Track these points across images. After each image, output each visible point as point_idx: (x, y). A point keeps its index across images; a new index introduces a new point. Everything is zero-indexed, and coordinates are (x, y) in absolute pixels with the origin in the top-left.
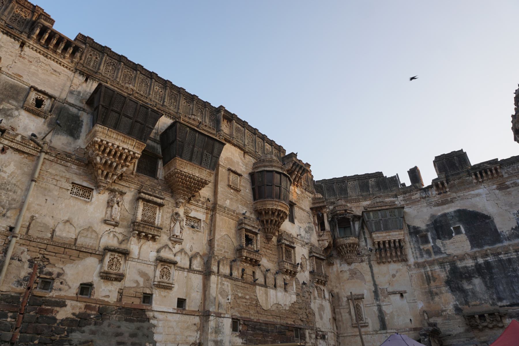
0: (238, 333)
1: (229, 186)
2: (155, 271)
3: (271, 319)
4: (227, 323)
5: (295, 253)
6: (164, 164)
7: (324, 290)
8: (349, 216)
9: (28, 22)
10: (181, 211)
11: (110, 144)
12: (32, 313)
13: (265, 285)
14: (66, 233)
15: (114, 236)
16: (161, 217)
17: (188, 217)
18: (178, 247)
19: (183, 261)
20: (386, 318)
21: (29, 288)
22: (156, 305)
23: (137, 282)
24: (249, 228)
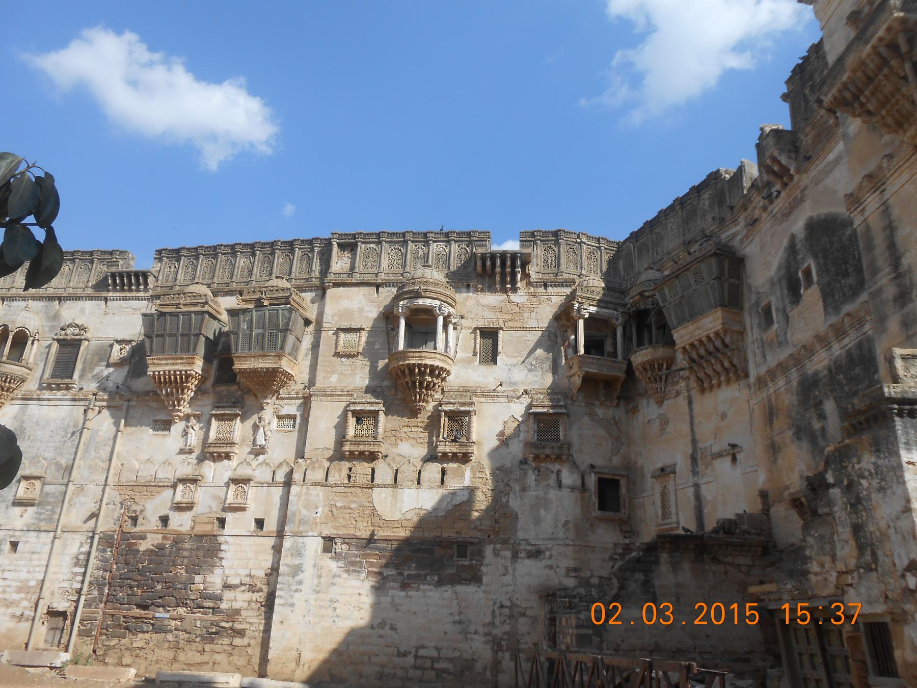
1: (337, 355)
14: (147, 473)
20: (705, 511)
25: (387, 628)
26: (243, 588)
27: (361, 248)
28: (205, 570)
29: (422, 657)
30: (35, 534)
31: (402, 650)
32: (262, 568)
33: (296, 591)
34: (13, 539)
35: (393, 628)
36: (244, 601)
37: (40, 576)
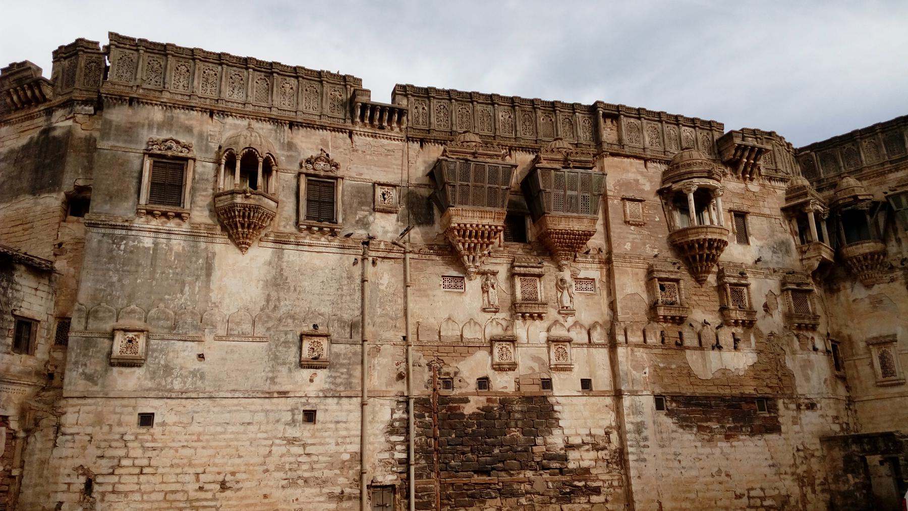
0: (665, 412)
1: (627, 223)
2: (549, 352)
3: (715, 391)
4: (648, 402)
5: (748, 293)
6: (534, 221)
7: (813, 338)
8: (864, 206)
9: (346, 103)
10: (567, 275)
11: (468, 226)
12: (444, 411)
13: (701, 347)
14: (450, 332)
15: (498, 323)
16: (544, 289)
17: (577, 280)
18: (571, 320)
19: (579, 336)
21: (434, 390)
22: (556, 390)
23: (531, 368)
24: (663, 275)
25: (723, 475)
26: (587, 447)
27: (624, 121)
28: (543, 431)
29: (753, 497)
30: (336, 400)
31: (738, 492)
32: (600, 427)
33: (644, 446)
34: (308, 408)
35: (728, 475)
36: (590, 460)
37: (356, 448)
